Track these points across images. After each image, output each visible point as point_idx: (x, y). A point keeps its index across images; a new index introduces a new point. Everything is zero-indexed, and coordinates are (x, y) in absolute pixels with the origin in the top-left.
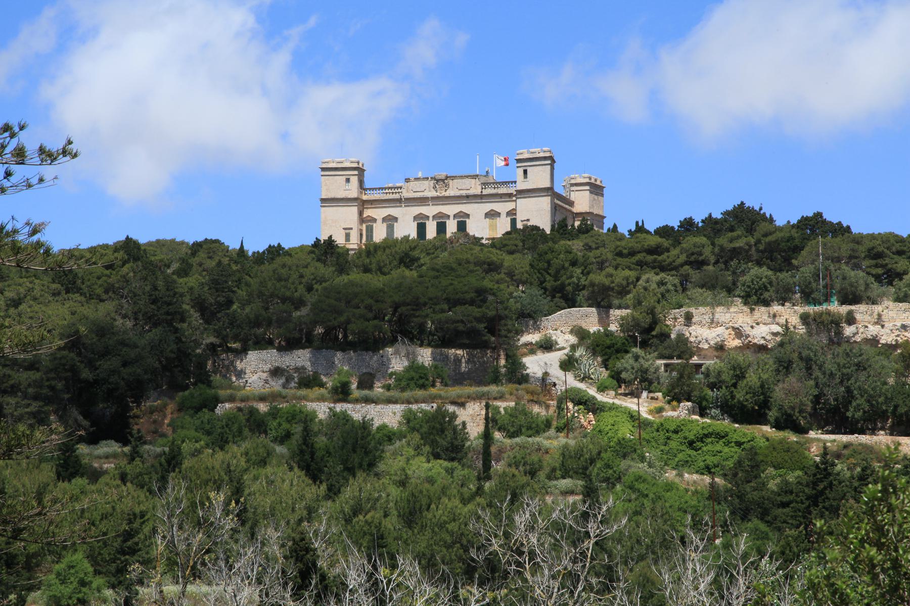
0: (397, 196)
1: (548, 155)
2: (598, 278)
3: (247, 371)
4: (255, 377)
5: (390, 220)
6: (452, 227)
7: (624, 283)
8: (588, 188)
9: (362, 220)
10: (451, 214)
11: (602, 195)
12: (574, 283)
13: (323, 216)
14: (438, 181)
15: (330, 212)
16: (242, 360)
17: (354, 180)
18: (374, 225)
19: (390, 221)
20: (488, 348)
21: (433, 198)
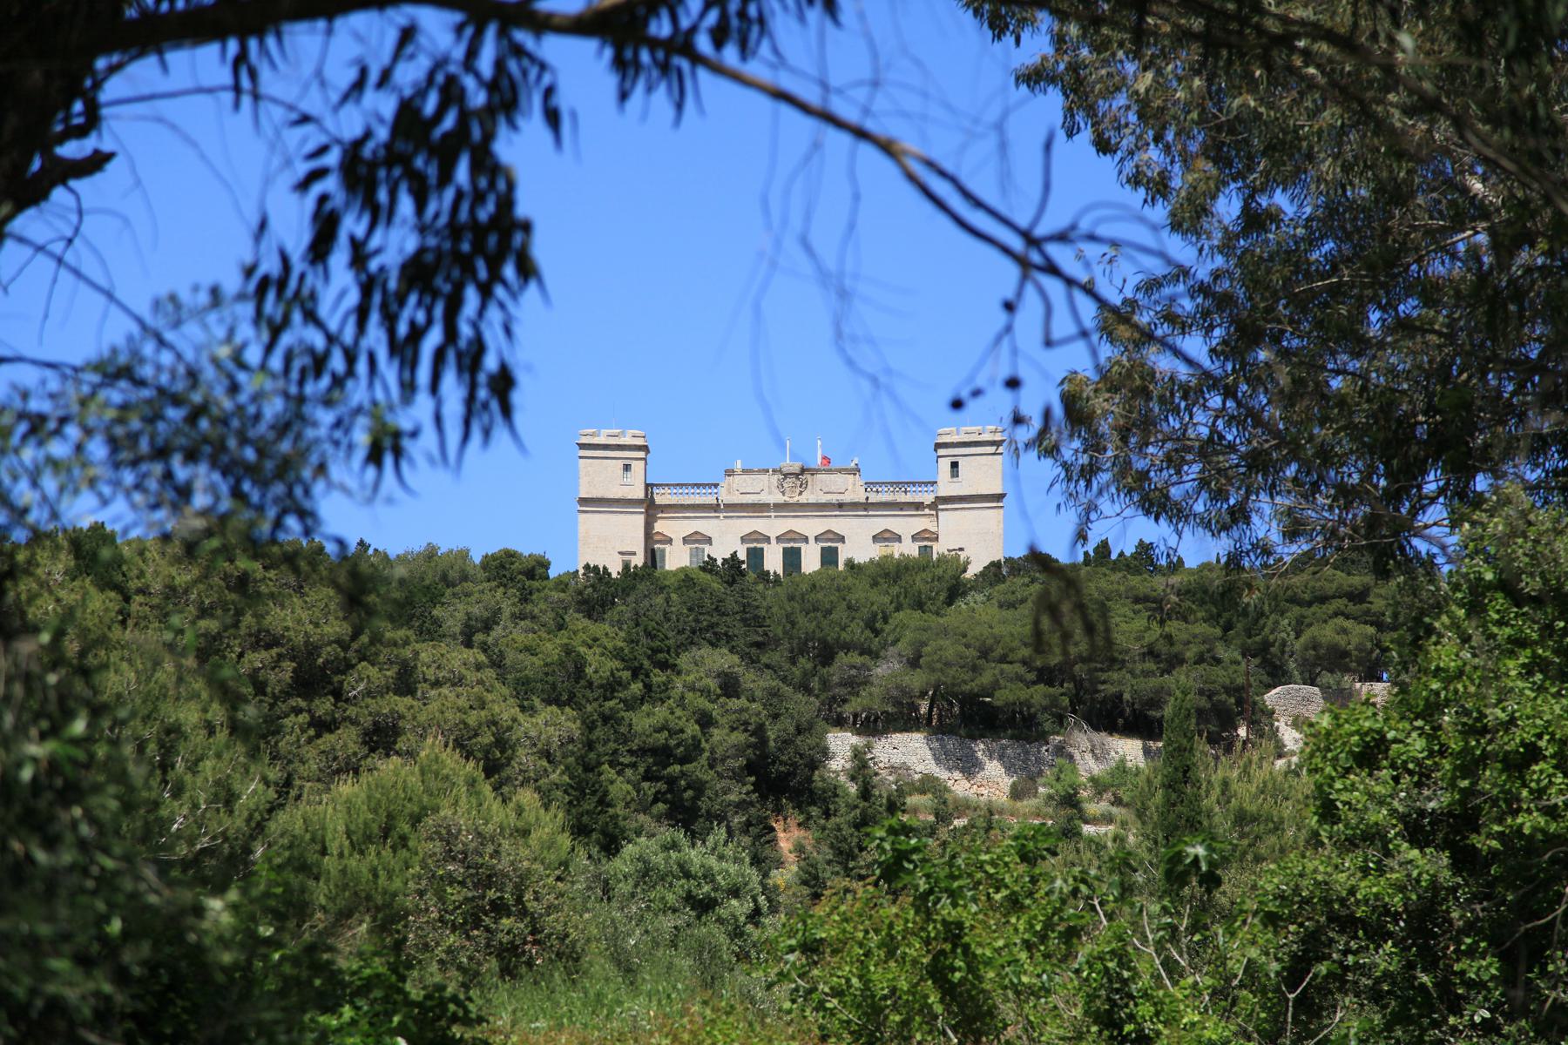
0: (711, 500)
1: (640, 442)
6: (811, 562)
13: (581, 529)
15: (593, 524)
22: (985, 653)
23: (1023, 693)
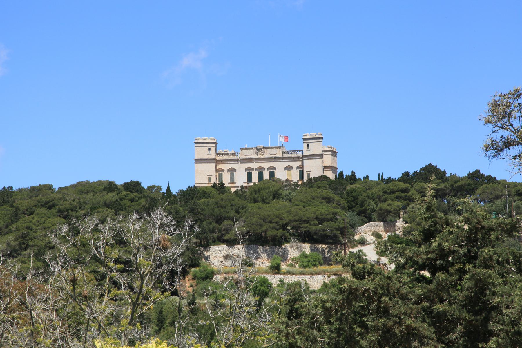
0: (236, 158)
1: (213, 141)
2: (385, 206)
3: (211, 257)
4: (216, 260)
5: (232, 170)
6: (266, 176)
7: (398, 209)
8: (330, 153)
9: (217, 171)
10: (266, 167)
11: (336, 157)
12: (371, 208)
14: (258, 150)
16: (208, 251)
17: (213, 149)
18: (223, 173)
19: (232, 171)
20: (338, 244)
21: (256, 159)
22: (264, 220)
23: (275, 232)
